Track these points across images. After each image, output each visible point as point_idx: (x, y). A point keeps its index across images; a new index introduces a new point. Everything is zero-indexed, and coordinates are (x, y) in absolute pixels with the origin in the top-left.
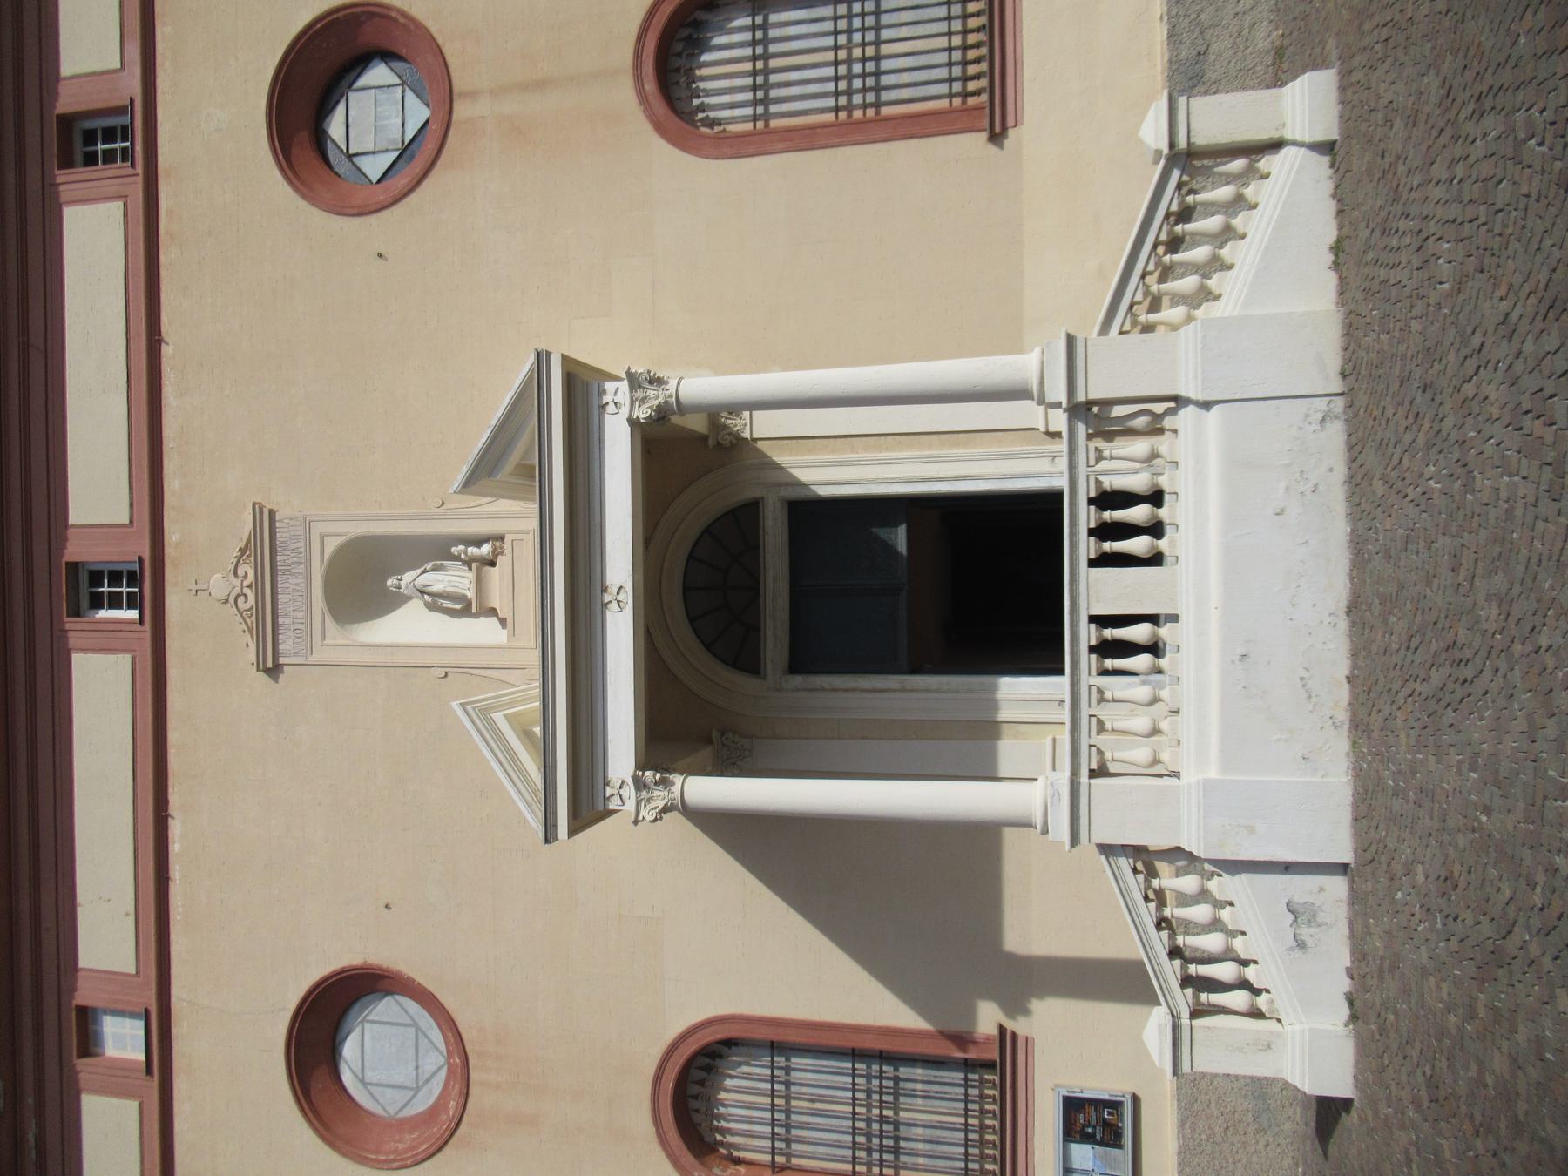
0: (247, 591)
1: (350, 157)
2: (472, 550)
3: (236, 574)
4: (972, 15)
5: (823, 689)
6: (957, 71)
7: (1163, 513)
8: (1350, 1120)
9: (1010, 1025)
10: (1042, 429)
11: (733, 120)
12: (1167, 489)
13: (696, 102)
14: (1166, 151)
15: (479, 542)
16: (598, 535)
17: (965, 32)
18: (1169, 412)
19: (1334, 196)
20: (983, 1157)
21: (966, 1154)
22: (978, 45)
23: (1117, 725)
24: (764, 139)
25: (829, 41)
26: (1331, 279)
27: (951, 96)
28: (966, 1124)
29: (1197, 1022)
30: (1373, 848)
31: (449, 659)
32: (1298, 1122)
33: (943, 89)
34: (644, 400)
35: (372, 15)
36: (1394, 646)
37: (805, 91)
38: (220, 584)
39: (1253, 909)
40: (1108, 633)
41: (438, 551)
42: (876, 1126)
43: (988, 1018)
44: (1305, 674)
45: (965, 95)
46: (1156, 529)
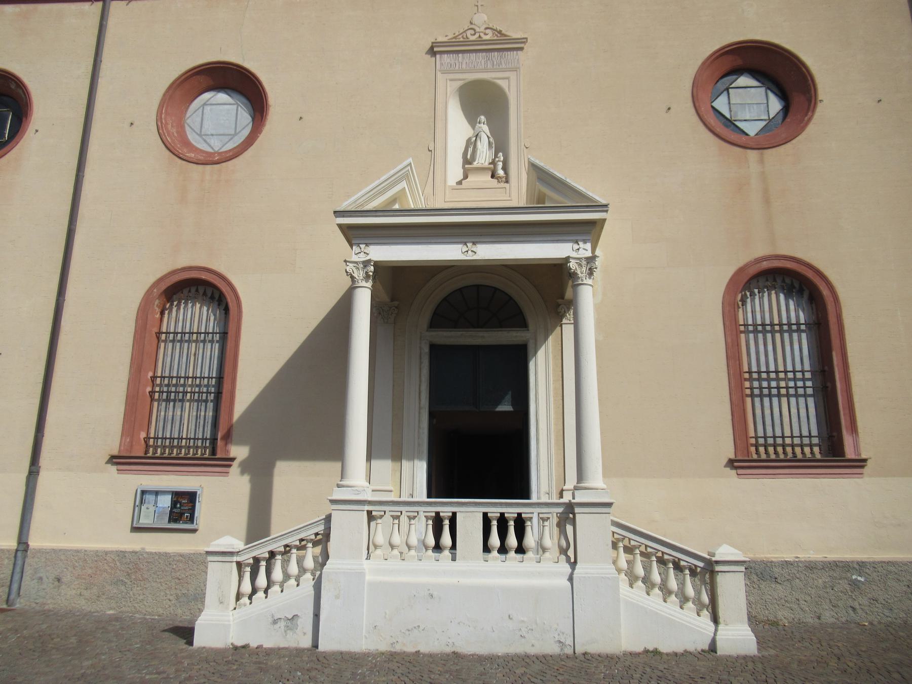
0: (477, 35)
1: (727, 89)
2: (500, 165)
3: (486, 28)
4: (812, 450)
5: (421, 363)
6: (770, 441)
7: (512, 554)
8: (182, 644)
9: (235, 464)
10: (565, 488)
11: (745, 313)
12: (526, 556)
13: (756, 291)
14: (714, 559)
15: (505, 168)
16: (504, 239)
17: (793, 446)
18: (568, 558)
19: (686, 651)
20: (164, 447)
21: (166, 438)
22: (785, 453)
23: (413, 527)
24: (734, 330)
25: (790, 368)
26: (639, 649)
27: (756, 438)
28: (182, 439)
29: (234, 565)
30: (325, 661)
31: (439, 153)
32: (181, 616)
33: (760, 433)
34: (580, 265)
35: (809, 101)
36: (432, 676)
37: (760, 354)
38: (481, 19)
39: (293, 597)
40: (447, 522)
41: (500, 145)
42: (181, 389)
43: (239, 452)
44: (421, 628)
45: (757, 446)
46: (503, 550)
